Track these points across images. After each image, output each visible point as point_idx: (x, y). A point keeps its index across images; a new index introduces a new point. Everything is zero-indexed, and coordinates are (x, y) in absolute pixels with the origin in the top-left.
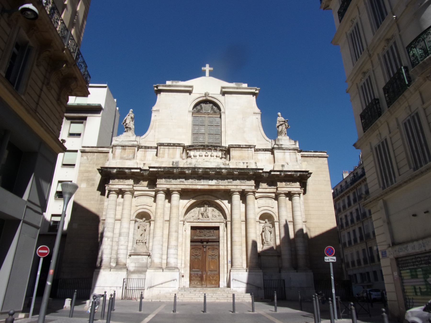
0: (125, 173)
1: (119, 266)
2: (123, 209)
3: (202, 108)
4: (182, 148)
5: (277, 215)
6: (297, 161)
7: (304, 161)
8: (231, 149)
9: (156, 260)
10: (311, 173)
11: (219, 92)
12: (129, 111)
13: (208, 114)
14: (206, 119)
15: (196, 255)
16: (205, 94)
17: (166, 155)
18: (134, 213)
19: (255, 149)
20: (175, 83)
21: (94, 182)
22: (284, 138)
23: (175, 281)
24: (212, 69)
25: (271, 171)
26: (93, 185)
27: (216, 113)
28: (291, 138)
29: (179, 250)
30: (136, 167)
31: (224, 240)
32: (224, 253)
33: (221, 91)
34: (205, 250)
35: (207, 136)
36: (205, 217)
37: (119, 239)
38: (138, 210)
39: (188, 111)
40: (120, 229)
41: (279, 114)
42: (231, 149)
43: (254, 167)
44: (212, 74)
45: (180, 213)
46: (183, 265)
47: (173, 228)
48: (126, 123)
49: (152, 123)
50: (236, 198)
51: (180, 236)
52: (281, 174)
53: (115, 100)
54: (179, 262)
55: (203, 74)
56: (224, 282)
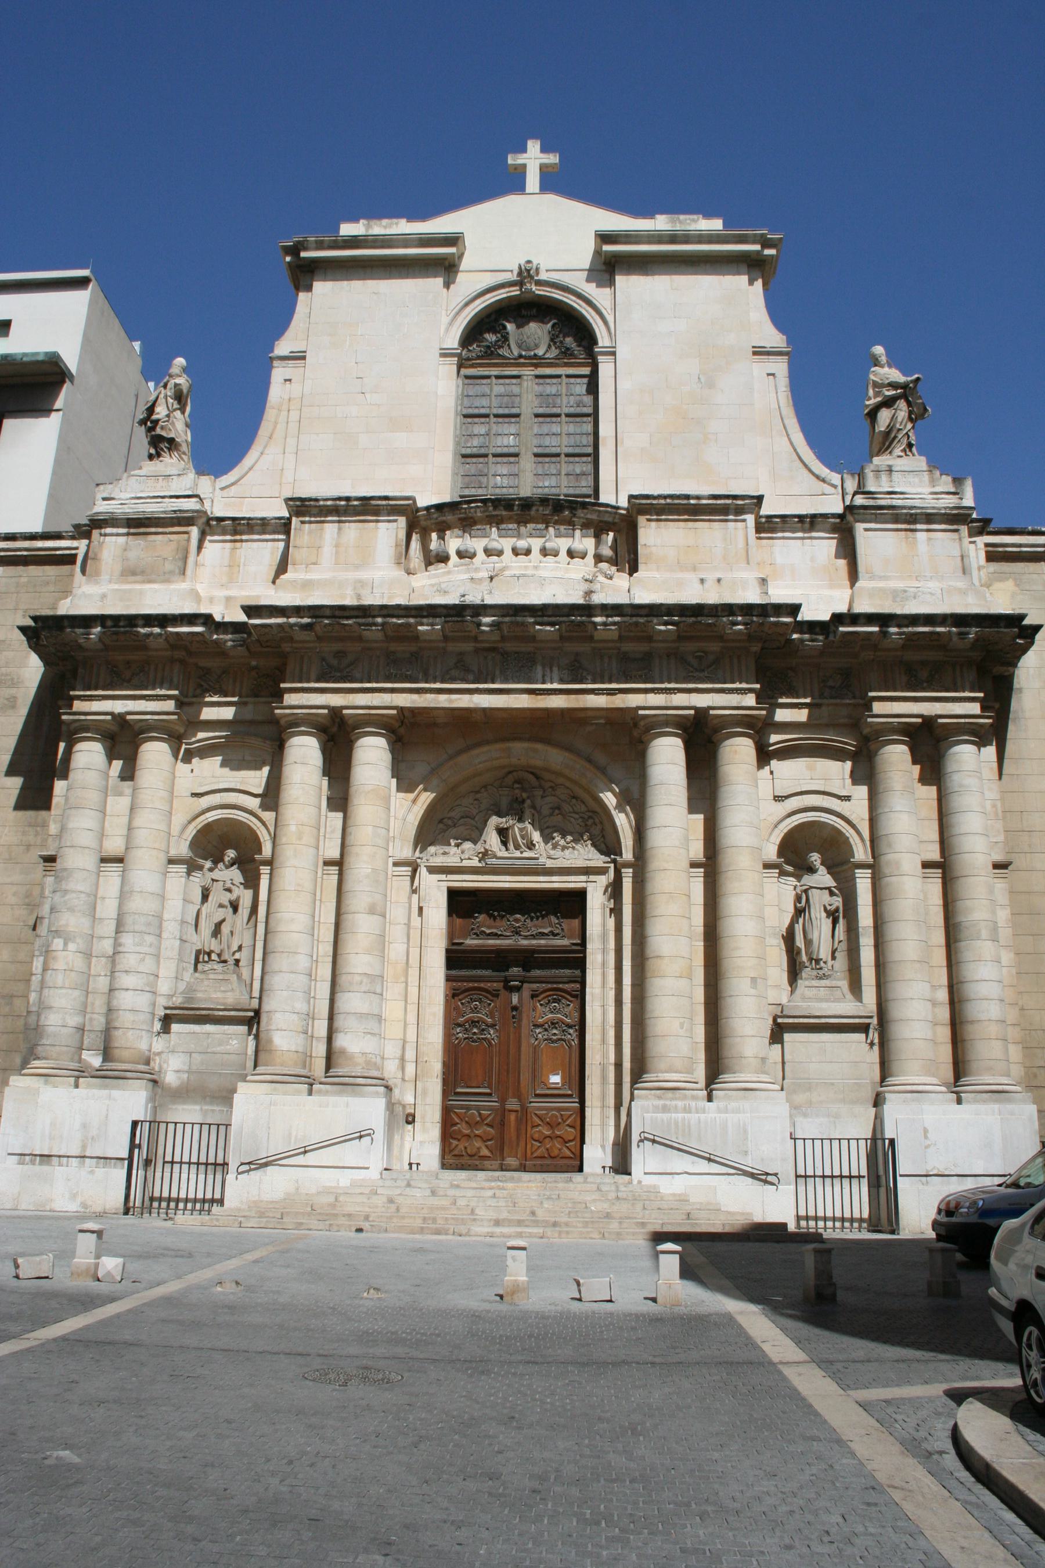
0: (142, 644)
1: (107, 1059)
2: (132, 809)
3: (505, 338)
4: (402, 521)
5: (866, 834)
6: (965, 571)
7: (1001, 577)
8: (642, 520)
9: (285, 1034)
10: (1037, 628)
11: (585, 259)
12: (169, 365)
13: (537, 361)
14: (528, 392)
15: (474, 1023)
16: (520, 274)
17: (327, 551)
18: (185, 828)
19: (758, 517)
20: (380, 228)
21: (13, 691)
22: (899, 461)
23: (366, 1140)
24: (553, 159)
25: (838, 618)
26: (12, 703)
27: (572, 355)
28: (937, 465)
29: (388, 995)
30: (188, 609)
31: (604, 951)
32: (604, 1014)
33: (598, 253)
34: (515, 999)
35: (527, 463)
36: (517, 847)
37: (117, 944)
38: (203, 812)
39: (437, 352)
40: (123, 896)
41: (879, 350)
42: (642, 520)
43: (753, 596)
44: (551, 182)
45: (395, 825)
46: (410, 1069)
47: (360, 897)
48: (154, 417)
49: (270, 414)
50: (668, 756)
51: (396, 933)
52: (884, 634)
53: (137, 345)
54: (392, 1050)
55: (514, 182)
56: (603, 1147)
